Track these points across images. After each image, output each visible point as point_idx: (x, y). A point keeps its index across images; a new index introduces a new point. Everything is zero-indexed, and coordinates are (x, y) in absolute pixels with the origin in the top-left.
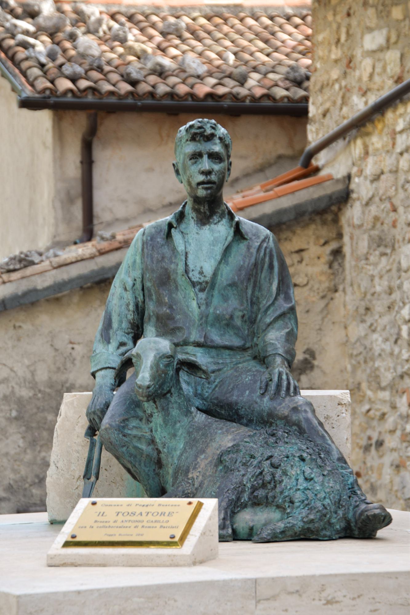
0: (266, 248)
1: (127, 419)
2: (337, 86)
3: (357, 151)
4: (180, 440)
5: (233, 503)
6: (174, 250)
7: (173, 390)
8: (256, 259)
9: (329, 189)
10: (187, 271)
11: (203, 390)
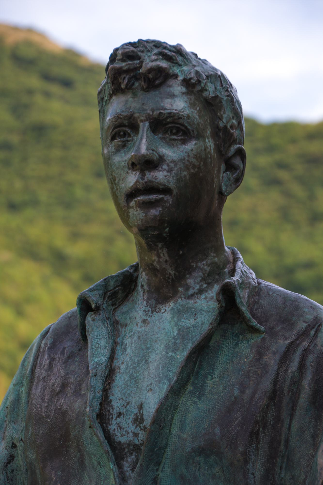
8: (275, 382)
10: (103, 417)
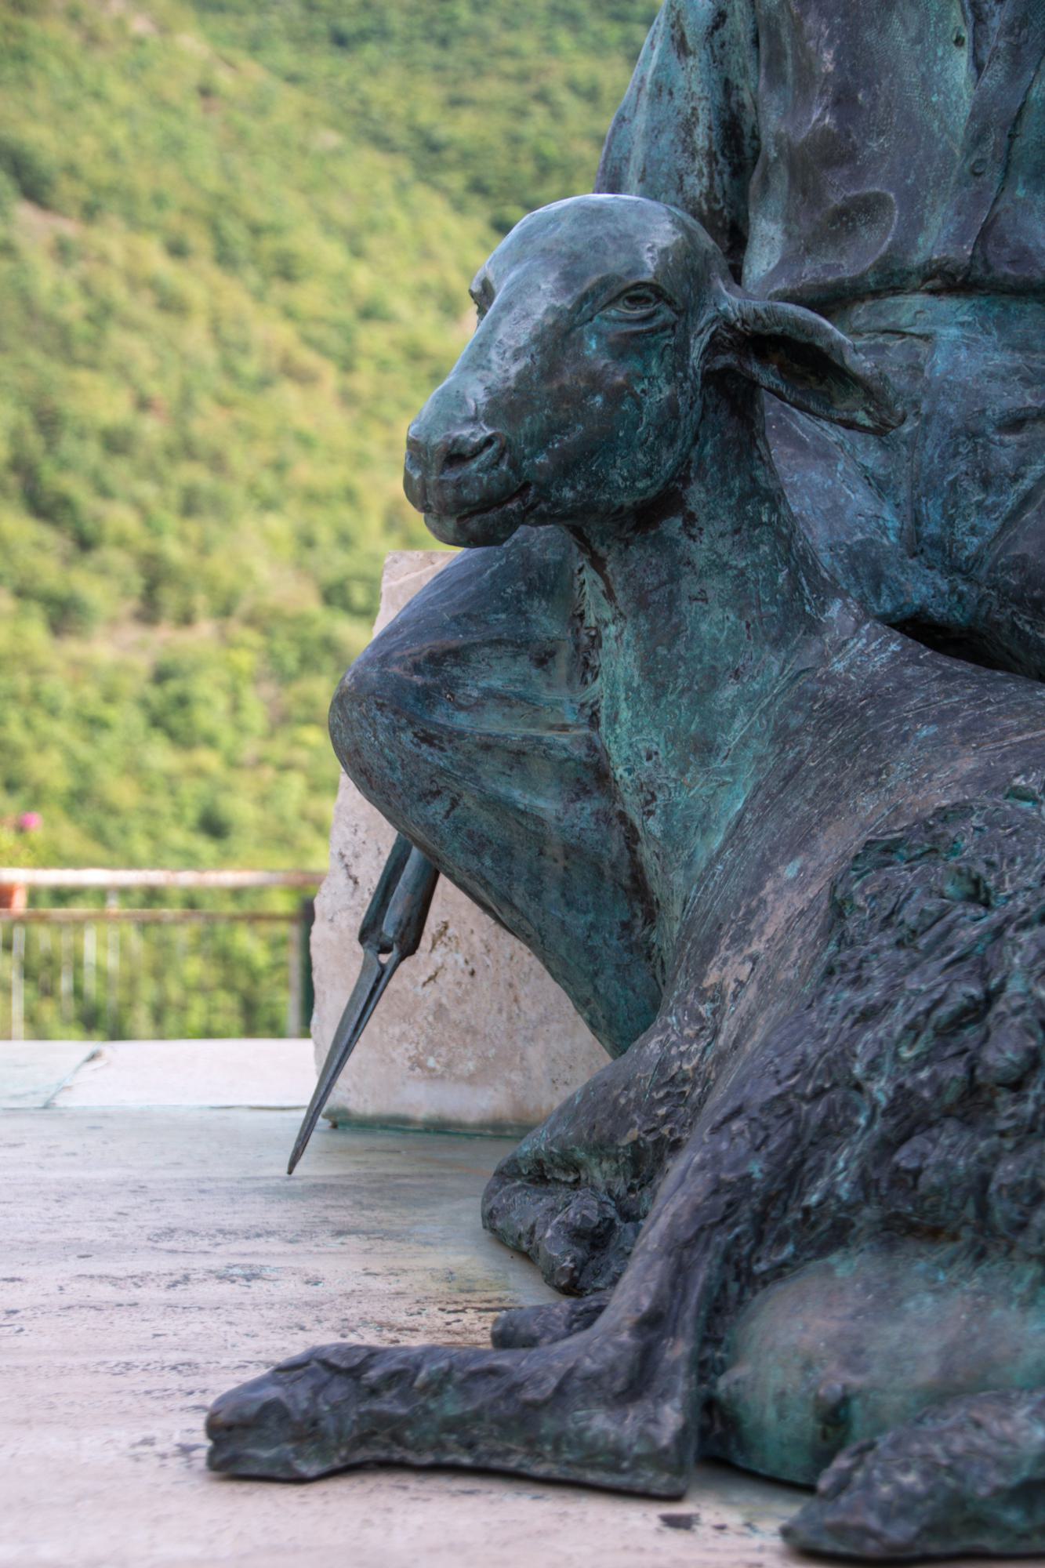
1: (458, 655)
4: (732, 771)
5: (745, 1211)
7: (697, 495)
11: (950, 521)
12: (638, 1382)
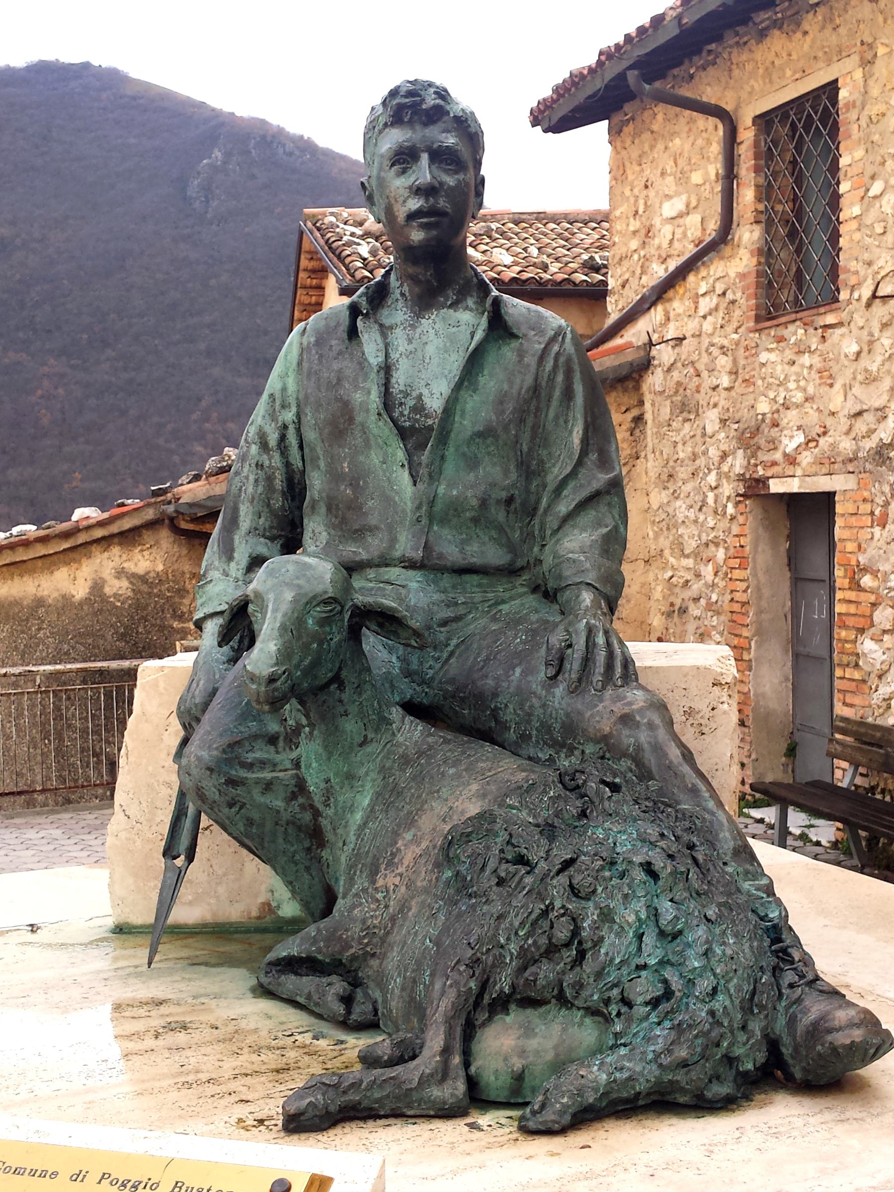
0: (558, 354)
2: (636, 257)
3: (658, 318)
6: (362, 362)
8: (536, 379)
9: (630, 356)
11: (421, 663)
12: (443, 1074)
